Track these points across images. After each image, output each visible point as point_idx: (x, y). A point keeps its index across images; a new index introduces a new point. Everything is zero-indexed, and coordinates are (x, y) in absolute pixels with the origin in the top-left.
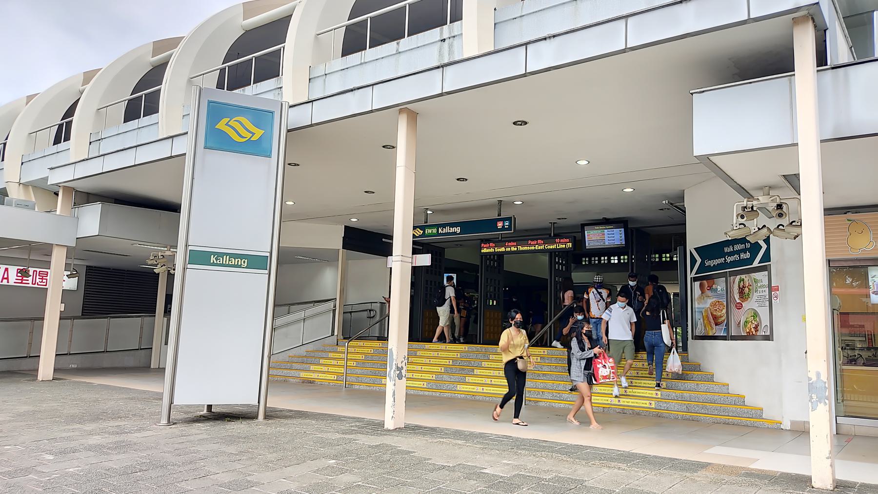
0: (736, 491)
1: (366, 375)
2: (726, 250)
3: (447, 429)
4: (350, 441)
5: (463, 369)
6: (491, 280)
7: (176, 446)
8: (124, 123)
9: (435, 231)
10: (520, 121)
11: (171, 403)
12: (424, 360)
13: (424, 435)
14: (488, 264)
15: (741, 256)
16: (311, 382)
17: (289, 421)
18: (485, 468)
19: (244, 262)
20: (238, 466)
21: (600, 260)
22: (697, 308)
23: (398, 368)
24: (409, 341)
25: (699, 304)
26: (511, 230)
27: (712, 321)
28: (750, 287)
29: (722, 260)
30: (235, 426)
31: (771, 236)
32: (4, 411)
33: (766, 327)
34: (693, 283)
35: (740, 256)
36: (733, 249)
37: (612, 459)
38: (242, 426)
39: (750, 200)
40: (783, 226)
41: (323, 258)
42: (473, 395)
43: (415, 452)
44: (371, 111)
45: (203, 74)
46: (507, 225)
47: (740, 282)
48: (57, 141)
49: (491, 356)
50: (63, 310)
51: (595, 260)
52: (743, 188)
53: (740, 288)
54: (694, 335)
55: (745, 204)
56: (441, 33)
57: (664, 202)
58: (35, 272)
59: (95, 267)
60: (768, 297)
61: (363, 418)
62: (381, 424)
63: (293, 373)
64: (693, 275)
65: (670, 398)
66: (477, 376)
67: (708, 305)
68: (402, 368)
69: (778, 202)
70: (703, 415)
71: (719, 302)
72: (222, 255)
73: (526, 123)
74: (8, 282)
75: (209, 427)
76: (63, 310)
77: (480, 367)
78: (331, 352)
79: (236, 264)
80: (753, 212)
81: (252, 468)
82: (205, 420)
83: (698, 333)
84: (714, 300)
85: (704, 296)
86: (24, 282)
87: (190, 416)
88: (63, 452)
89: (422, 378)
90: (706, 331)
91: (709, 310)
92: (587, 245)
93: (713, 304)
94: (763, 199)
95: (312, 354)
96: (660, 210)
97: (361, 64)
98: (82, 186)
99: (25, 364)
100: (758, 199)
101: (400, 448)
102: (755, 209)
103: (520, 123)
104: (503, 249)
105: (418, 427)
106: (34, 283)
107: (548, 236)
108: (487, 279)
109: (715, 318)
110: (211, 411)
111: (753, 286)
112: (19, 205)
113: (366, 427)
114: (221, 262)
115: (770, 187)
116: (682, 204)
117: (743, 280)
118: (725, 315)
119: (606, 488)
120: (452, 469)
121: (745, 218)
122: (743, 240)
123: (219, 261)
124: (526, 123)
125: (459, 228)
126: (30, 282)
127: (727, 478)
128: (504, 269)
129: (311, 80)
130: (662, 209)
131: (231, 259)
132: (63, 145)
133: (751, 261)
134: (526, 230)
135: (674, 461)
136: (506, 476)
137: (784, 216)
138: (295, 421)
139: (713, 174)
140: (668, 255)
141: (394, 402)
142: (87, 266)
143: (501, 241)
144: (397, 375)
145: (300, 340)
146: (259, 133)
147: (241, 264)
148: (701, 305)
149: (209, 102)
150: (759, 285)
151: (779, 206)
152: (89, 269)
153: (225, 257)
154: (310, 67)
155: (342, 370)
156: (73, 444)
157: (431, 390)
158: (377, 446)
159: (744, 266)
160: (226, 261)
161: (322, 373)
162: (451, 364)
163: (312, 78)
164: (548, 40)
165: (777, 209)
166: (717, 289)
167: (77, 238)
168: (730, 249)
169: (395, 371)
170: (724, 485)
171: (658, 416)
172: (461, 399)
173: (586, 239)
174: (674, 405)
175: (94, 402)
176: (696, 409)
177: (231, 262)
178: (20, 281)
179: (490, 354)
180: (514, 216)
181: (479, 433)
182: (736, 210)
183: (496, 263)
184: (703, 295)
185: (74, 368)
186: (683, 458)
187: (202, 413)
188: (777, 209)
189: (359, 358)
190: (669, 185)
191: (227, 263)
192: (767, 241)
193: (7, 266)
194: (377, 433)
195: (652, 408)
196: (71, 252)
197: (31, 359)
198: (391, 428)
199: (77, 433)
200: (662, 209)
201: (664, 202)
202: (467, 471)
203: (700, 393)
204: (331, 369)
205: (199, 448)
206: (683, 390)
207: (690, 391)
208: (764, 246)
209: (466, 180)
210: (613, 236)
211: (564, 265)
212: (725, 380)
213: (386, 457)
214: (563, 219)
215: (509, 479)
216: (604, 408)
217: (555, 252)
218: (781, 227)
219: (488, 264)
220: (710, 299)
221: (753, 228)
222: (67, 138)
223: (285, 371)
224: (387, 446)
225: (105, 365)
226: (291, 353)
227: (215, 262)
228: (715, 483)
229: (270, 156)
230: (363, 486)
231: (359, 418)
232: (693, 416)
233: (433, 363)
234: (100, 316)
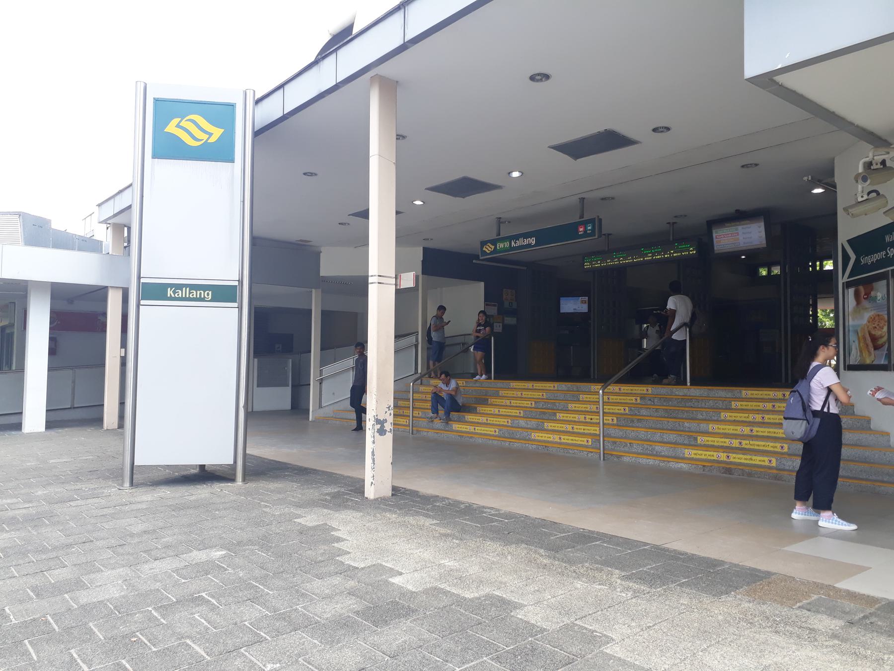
5: (544, 413)
9: (507, 244)
19: (208, 294)
23: (378, 421)
25: (853, 320)
27: (870, 344)
46: (589, 230)
49: (581, 396)
57: (805, 178)
64: (846, 279)
67: (865, 321)
68: (385, 421)
72: (180, 287)
79: (198, 296)
93: (872, 320)
109: (874, 339)
114: (195, 296)
123: (178, 295)
141: (374, 464)
153: (184, 289)
191: (187, 296)
201: (805, 178)
212: (885, 428)
227: (173, 296)
229: (232, 161)
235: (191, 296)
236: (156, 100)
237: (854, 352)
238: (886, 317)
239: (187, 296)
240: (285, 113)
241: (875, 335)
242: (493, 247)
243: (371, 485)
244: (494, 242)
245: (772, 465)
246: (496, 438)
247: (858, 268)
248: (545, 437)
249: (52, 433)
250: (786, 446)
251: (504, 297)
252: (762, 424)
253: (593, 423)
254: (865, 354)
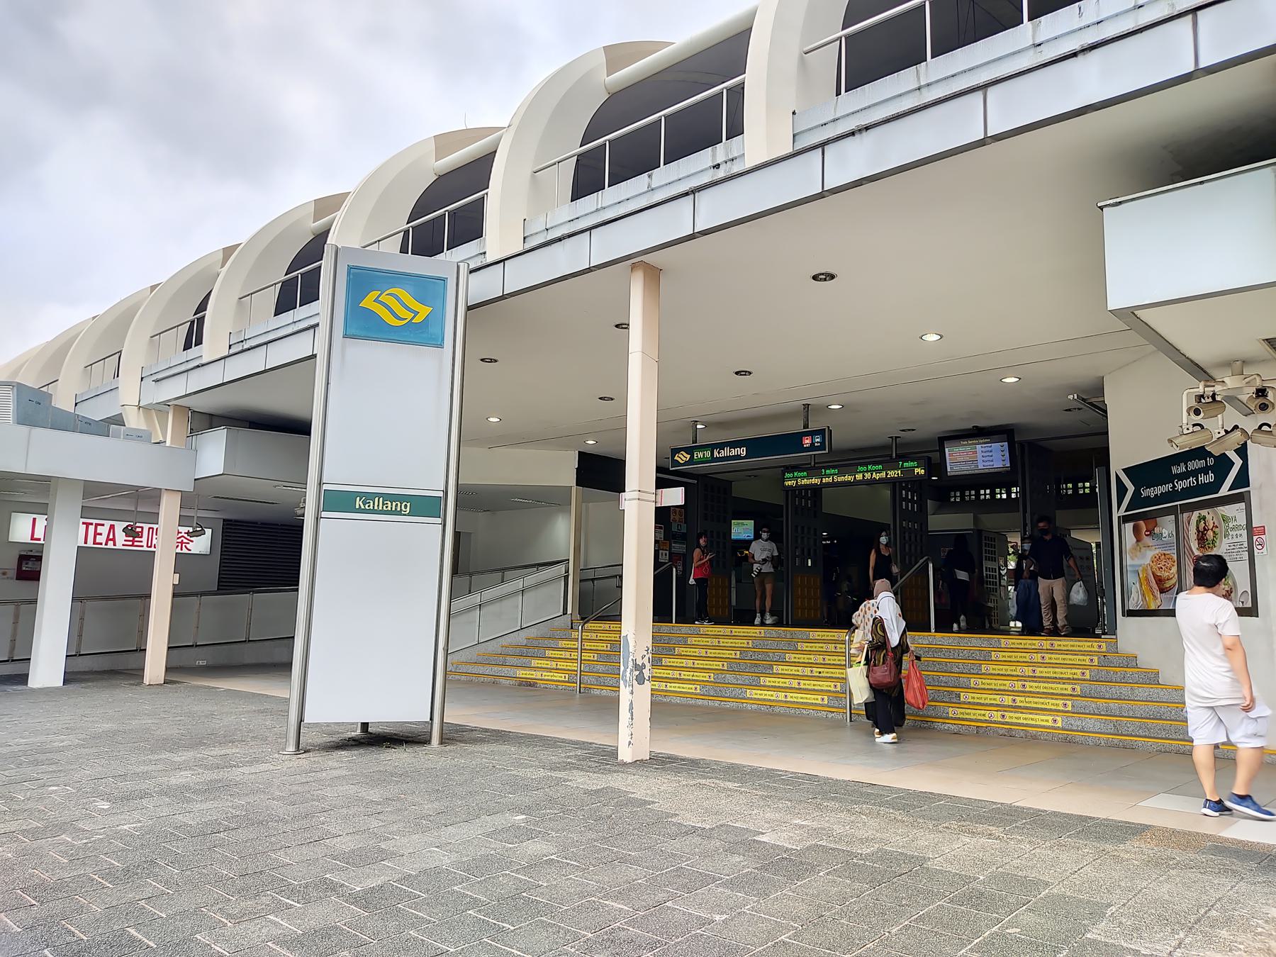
0: (1194, 882)
1: (611, 674)
2: (1175, 470)
3: (716, 763)
4: (559, 782)
5: (756, 666)
6: (803, 528)
7: (295, 788)
8: (275, 315)
9: (708, 454)
10: (823, 274)
11: (301, 720)
12: (697, 652)
13: (677, 771)
14: (797, 503)
15: (1200, 479)
16: (530, 684)
17: (477, 748)
18: (763, 834)
19: (406, 506)
20: (374, 823)
21: (978, 495)
22: (1130, 566)
23: (636, 667)
24: (653, 622)
26: (825, 450)
28: (1216, 530)
29: (1167, 487)
30: (394, 755)
31: (1249, 442)
32: (77, 731)
33: (1245, 594)
34: (1123, 526)
35: (1197, 480)
36: (1186, 468)
37: (980, 819)
38: (405, 755)
39: (1209, 384)
40: (1270, 426)
41: (548, 500)
42: (770, 706)
43: (653, 802)
44: (589, 270)
45: (379, 241)
46: (818, 442)
47: (1198, 522)
48: (187, 346)
49: (799, 644)
50: (177, 583)
51: (970, 495)
52: (1197, 365)
53: (1198, 531)
54: (1126, 608)
55: (1201, 390)
56: (714, 156)
58: (151, 530)
59: (236, 521)
60: (1246, 546)
61: (591, 743)
62: (614, 753)
63: (506, 671)
64: (1122, 512)
65: (1088, 712)
66: (778, 675)
67: (1148, 561)
68: (644, 665)
69: (1258, 383)
70: (1142, 739)
71: (1165, 555)
72: (368, 497)
73: (832, 277)
74: (115, 545)
75: (355, 758)
76: (177, 583)
77: (783, 662)
78: (562, 639)
79: (394, 509)
80: (1216, 405)
81: (395, 828)
82: (355, 745)
83: (1132, 606)
84: (1157, 551)
85: (1141, 546)
86: (136, 544)
87: (334, 739)
88: (126, 798)
89: (694, 678)
90: (1145, 603)
91: (1149, 568)
92: (949, 470)
93: (1157, 559)
94: (1231, 382)
95: (535, 643)
96: (1066, 410)
97: (597, 210)
98: (202, 404)
99: (130, 661)
100: (1223, 382)
101: (633, 796)
102: (1218, 398)
103: (824, 277)
104: (815, 481)
105: (672, 759)
106: (149, 545)
107: (889, 458)
108: (797, 527)
109: (1159, 581)
110: (367, 731)
111: (1221, 527)
112: (139, 436)
113: (591, 758)
115: (1244, 362)
116: (1101, 399)
117: (1204, 518)
118: (1176, 576)
119: (963, 873)
120: (706, 834)
121: (1202, 415)
122: (1200, 453)
123: (369, 506)
124: (832, 277)
125: (745, 449)
126: (144, 544)
127: (1179, 856)
128: (733, 495)
129: (526, 240)
130: (1070, 410)
131: (385, 502)
132: (194, 351)
133: (1216, 486)
134: (854, 450)
135: (1086, 821)
136: (794, 847)
137: (1270, 409)
138: (485, 748)
139: (1151, 348)
140: (1087, 484)
141: (632, 719)
142: (224, 520)
143: (814, 468)
144: (634, 677)
145: (517, 622)
146: (424, 311)
147: (401, 510)
148: (1136, 559)
149: (350, 268)
150: (1231, 525)
151: (1261, 392)
152: (227, 524)
153: (377, 499)
154: (525, 220)
155: (574, 666)
156: (146, 785)
157: (706, 698)
158: (597, 791)
159: (1204, 495)
160: (378, 506)
161: (547, 672)
162: (738, 657)
163: (528, 236)
164: (857, 136)
165: (1258, 396)
166: (1162, 534)
167: (195, 480)
168: (1181, 469)
169: (632, 671)
170: (1173, 869)
171: (1068, 741)
172: (751, 711)
173: (948, 461)
174: (1091, 722)
175: (206, 717)
176: (1130, 729)
177: (387, 507)
178: (131, 543)
179: (798, 642)
180: (829, 427)
181: (768, 769)
182: (1186, 401)
183: (809, 501)
184: (1140, 543)
185: (201, 666)
186: (1103, 816)
187: (353, 734)
188: (1258, 396)
189: (602, 648)
190: (1079, 369)
191: (380, 508)
192: (1242, 451)
193: (112, 523)
194: (605, 769)
195: (1058, 728)
196: (187, 500)
197: (251, 644)
198: (628, 759)
199: (160, 767)
200: (1070, 410)
201: (1071, 397)
202: (731, 838)
203: (1136, 702)
204: (562, 665)
205: (328, 792)
206: (1109, 699)
207: (1120, 699)
208: (1238, 462)
209: (750, 373)
210: (990, 454)
211: (915, 502)
213: (607, 811)
214: (909, 430)
215: (800, 853)
216: (977, 727)
217: (901, 483)
218: (1265, 428)
219: (797, 503)
220: (1151, 550)
221: (1218, 431)
222: (199, 342)
223: (496, 668)
224: (613, 790)
225: (248, 660)
226: (504, 641)
227: (363, 507)
228: (1157, 864)
230: (558, 861)
231: (584, 743)
232: (1125, 740)
233: (711, 655)
234: (245, 590)
237: (1134, 595)
238: (1175, 557)
241: (1161, 576)
242: (688, 456)
243: (629, 745)
244: (689, 450)
245: (1058, 725)
246: (698, 697)
247: (1136, 501)
248: (766, 695)
249: (70, 687)
250: (1069, 703)
251: (672, 517)
252: (1034, 678)
253: (822, 677)
254: (1149, 597)
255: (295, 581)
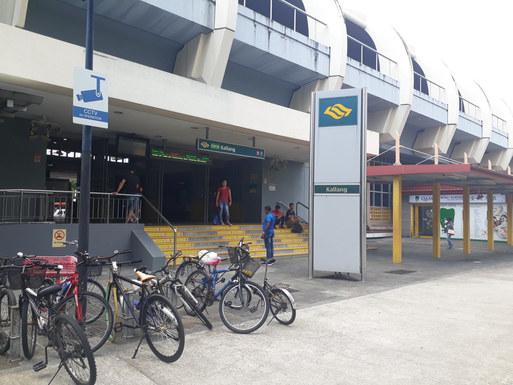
9: (218, 147)
19: (345, 190)
72: (332, 187)
79: (341, 191)
114: (339, 191)
123: (331, 190)
153: (334, 188)
163: (269, 33)
191: (336, 191)
235: (337, 191)
236: (355, 123)
239: (336, 191)
240: (205, 309)
255: (288, 228)
